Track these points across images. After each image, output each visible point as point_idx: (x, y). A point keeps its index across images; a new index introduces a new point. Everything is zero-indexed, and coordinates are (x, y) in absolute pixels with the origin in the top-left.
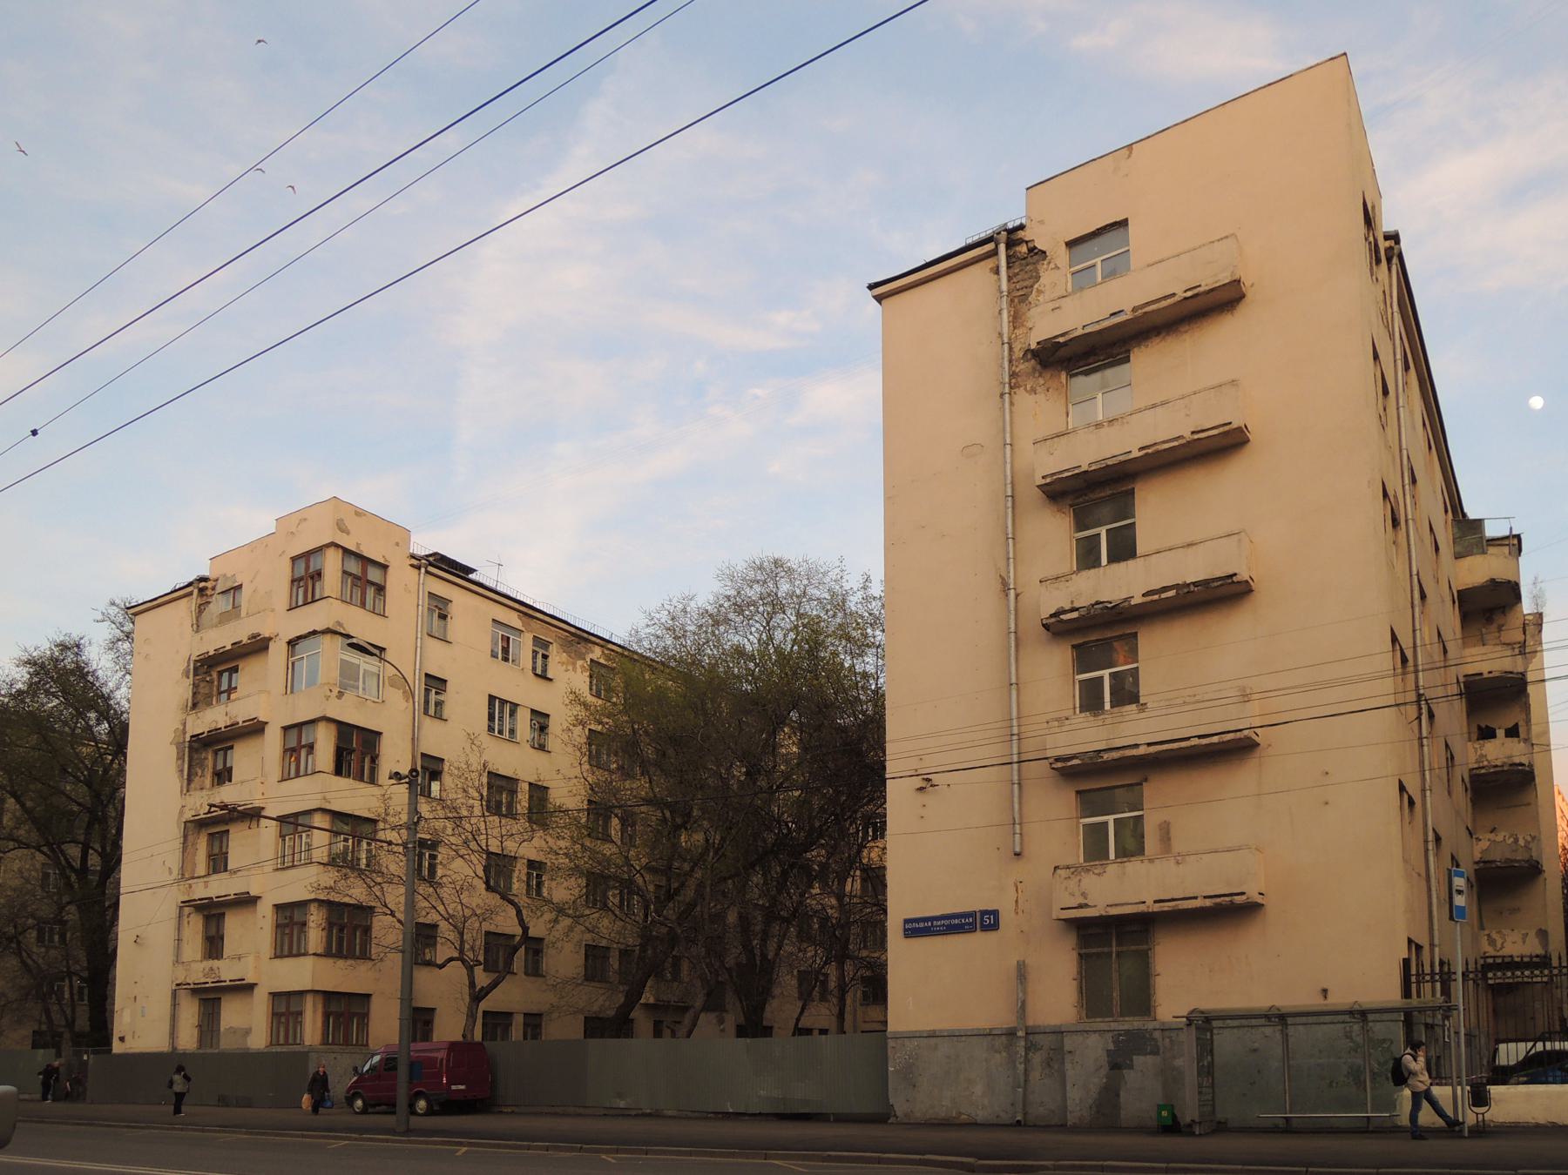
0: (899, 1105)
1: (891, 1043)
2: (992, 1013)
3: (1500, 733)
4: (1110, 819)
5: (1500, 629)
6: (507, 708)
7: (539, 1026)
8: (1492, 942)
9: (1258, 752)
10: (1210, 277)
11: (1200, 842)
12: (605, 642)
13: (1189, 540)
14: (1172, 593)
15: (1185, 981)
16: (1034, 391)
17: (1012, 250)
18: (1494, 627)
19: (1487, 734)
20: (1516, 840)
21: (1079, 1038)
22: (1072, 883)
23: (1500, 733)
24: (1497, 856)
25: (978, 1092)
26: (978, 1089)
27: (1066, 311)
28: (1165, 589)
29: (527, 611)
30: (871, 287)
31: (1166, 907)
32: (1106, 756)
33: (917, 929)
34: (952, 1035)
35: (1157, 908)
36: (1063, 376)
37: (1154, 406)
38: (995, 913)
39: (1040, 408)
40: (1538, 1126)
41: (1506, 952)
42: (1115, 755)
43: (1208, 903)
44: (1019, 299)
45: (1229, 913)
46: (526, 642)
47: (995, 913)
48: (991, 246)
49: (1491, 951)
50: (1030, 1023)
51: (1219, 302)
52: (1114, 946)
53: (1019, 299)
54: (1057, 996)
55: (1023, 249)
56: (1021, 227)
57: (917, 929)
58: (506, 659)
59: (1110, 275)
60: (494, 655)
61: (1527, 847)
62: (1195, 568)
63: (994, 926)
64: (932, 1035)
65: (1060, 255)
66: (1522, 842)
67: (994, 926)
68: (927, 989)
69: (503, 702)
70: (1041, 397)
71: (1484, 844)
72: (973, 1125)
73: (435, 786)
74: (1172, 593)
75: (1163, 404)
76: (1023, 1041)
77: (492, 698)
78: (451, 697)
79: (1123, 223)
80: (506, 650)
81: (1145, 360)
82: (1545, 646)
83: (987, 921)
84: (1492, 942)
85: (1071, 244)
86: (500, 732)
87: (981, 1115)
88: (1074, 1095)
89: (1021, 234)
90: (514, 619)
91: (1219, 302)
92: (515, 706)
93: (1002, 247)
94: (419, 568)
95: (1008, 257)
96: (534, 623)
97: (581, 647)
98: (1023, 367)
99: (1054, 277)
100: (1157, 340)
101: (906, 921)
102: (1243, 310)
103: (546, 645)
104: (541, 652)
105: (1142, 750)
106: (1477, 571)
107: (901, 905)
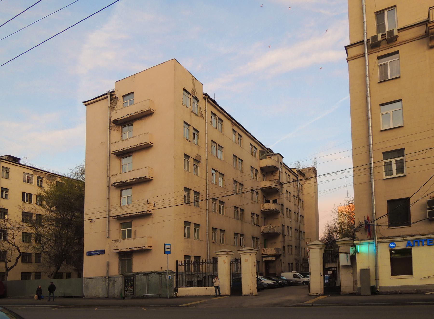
0: (85, 294)
1: (84, 280)
2: (103, 273)
3: (271, 201)
4: (126, 229)
5: (274, 176)
6: (29, 195)
7: (40, 275)
8: (264, 251)
9: (152, 216)
10: (145, 109)
11: (144, 235)
12: (61, 177)
13: (138, 168)
14: (135, 180)
15: (139, 265)
16: (115, 130)
17: (111, 96)
18: (273, 176)
19: (268, 202)
20: (271, 227)
21: (117, 278)
22: (115, 244)
23: (271, 201)
24: (265, 231)
25: (99, 290)
26: (100, 290)
27: (121, 113)
28: (134, 179)
29: (35, 170)
30: (84, 102)
31: (131, 250)
32: (122, 216)
33: (90, 254)
34: (95, 278)
35: (130, 250)
36: (120, 127)
37: (133, 137)
38: (104, 250)
39: (116, 134)
40: (196, 296)
41: (267, 253)
42: (123, 216)
43: (139, 249)
44: (112, 108)
45: (144, 251)
46: (35, 178)
47: (104, 250)
48: (107, 96)
49: (264, 253)
50: (110, 275)
51: (148, 114)
52: (125, 257)
53: (112, 108)
54: (115, 270)
55: (114, 96)
56: (113, 92)
57: (90, 254)
58: (29, 182)
59: (130, 105)
60: (24, 181)
61: (273, 229)
62: (139, 175)
63: (104, 253)
64: (92, 278)
65: (121, 99)
66: (272, 228)
67: (104, 253)
68: (92, 267)
69: (27, 194)
70: (116, 132)
71: (263, 228)
72: (99, 298)
73: (6, 217)
74: (135, 180)
75: (135, 137)
76: (109, 279)
77: (23, 193)
78: (10, 194)
79: (133, 93)
80: (29, 180)
81: (136, 125)
82: (352, 169)
83: (101, 252)
84: (264, 251)
85: (124, 96)
86: (27, 201)
87: (100, 296)
88: (116, 291)
89: (113, 93)
90: (31, 172)
91: (148, 114)
92: (31, 195)
93: (109, 96)
94: (205, 99)
95: (110, 98)
96: (37, 173)
97: (54, 178)
98: (113, 125)
99: (119, 104)
100: (138, 121)
101: (87, 252)
102: (154, 116)
103: (42, 178)
104: (40, 180)
105: (128, 215)
106: (267, 162)
107: (87, 248)
